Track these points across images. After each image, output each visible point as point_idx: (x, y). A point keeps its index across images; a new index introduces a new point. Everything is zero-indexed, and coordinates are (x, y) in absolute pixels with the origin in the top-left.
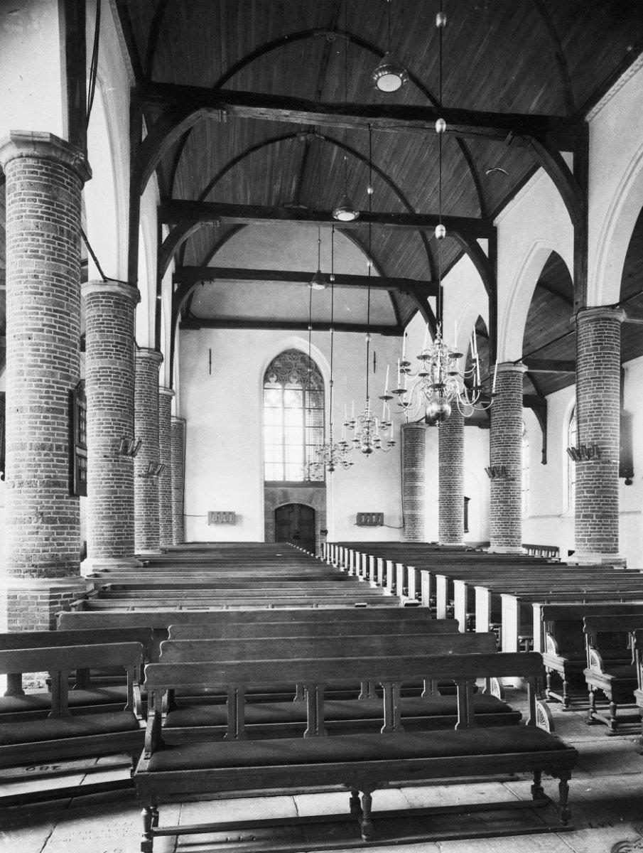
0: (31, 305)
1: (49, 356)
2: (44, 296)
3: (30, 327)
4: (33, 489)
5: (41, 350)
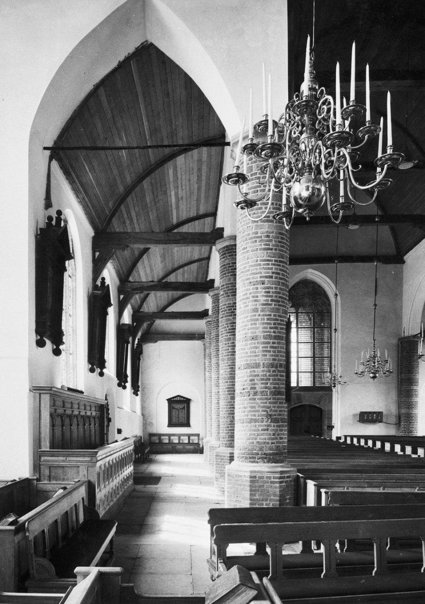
0: (265, 258)
1: (276, 296)
2: (274, 251)
3: (263, 275)
4: (265, 397)
5: (271, 292)
